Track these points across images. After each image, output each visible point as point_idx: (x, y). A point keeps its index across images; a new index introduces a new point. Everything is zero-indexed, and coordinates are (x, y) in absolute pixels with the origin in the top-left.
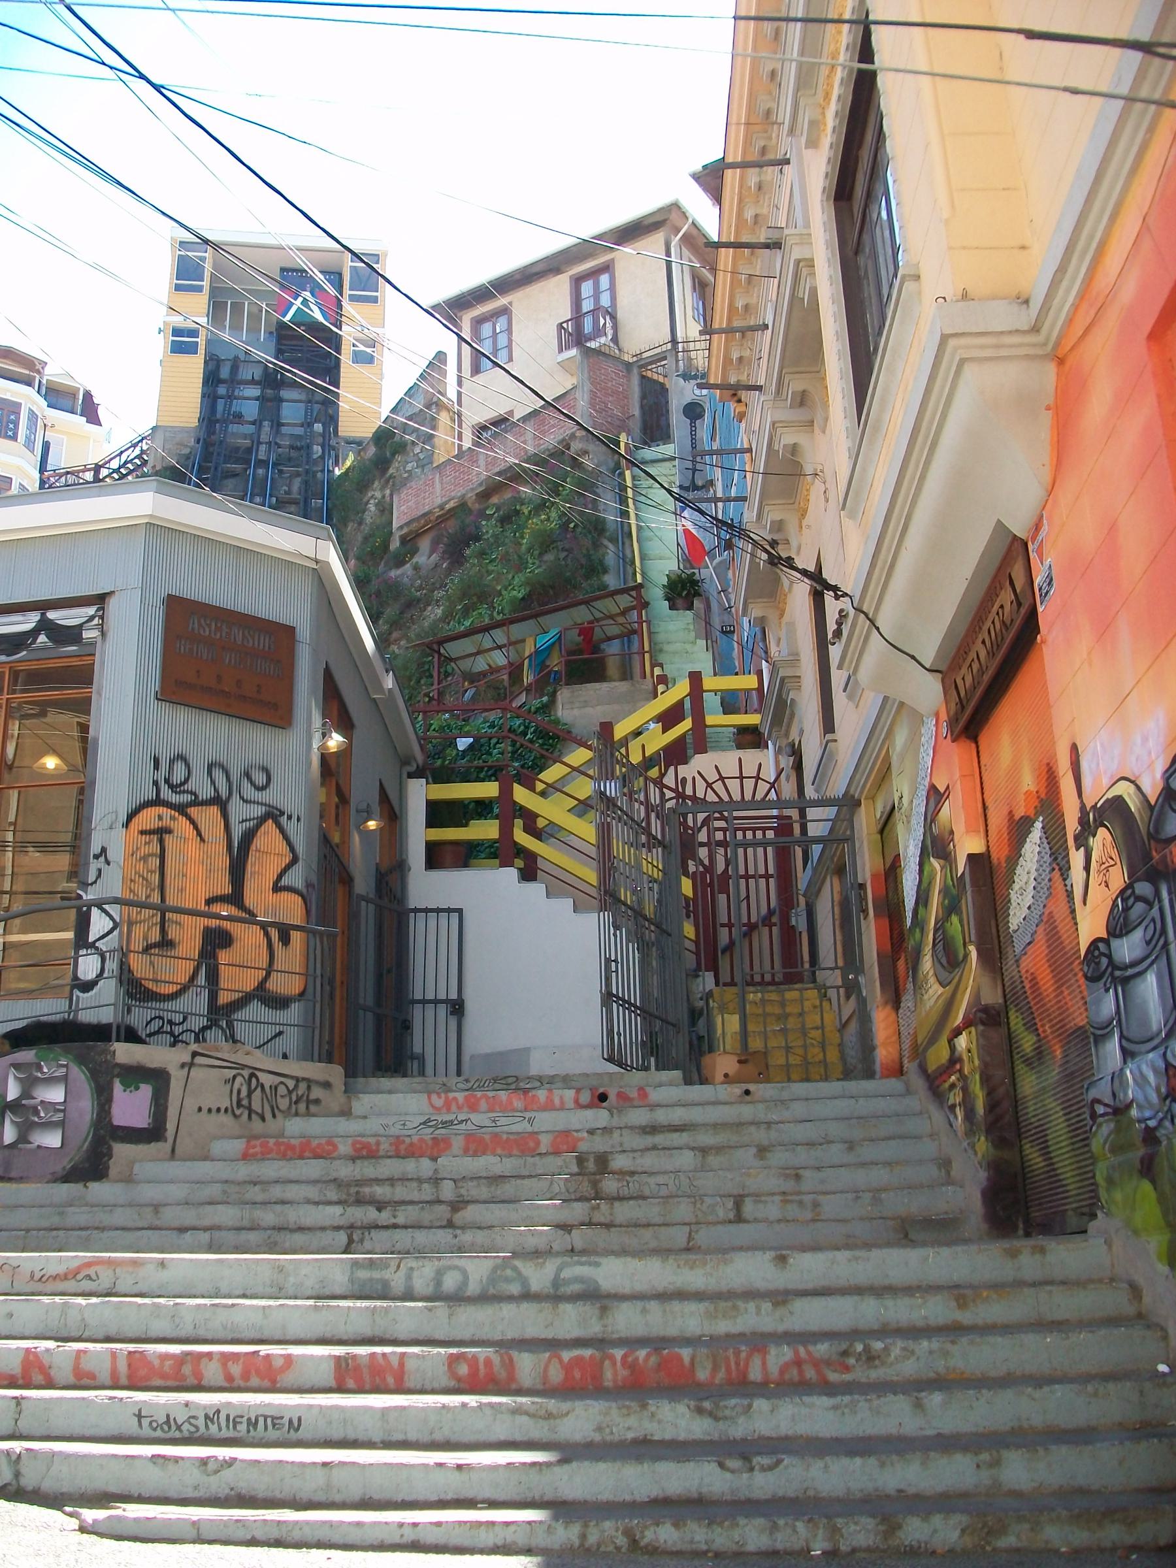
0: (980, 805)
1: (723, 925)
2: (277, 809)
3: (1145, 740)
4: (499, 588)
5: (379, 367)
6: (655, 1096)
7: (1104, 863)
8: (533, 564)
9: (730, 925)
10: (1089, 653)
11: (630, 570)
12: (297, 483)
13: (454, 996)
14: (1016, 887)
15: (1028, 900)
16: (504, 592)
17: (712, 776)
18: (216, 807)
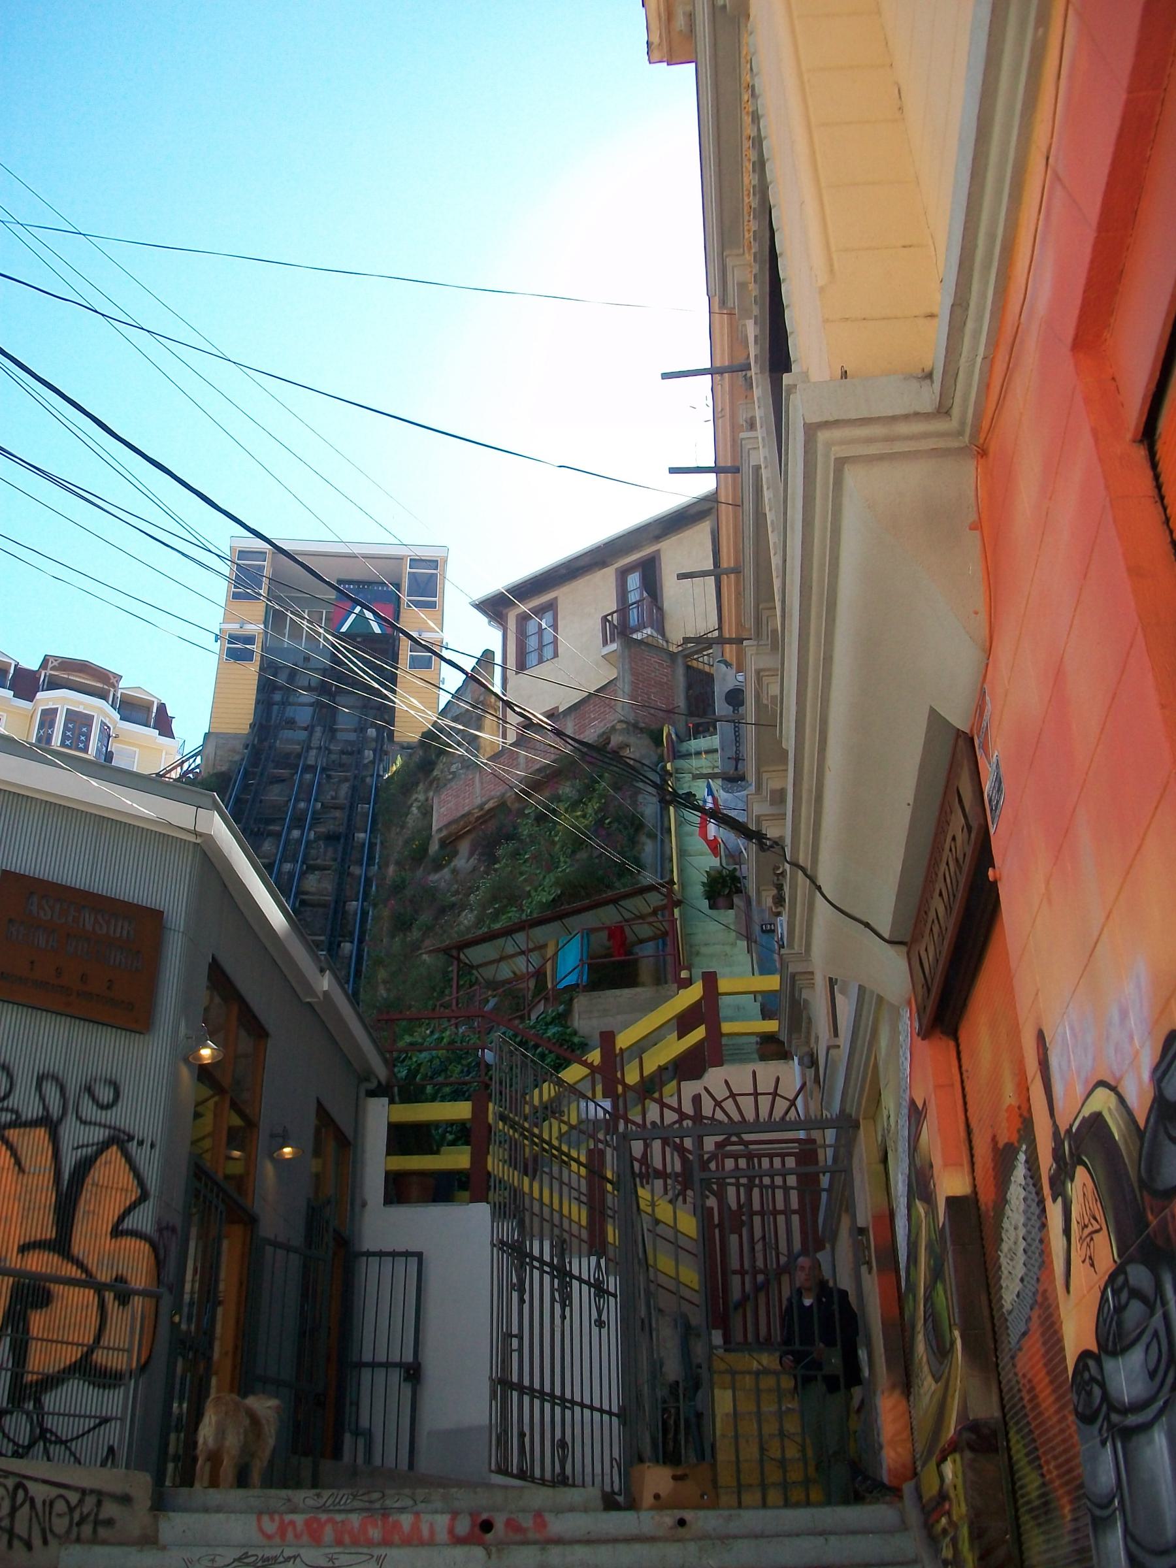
0: (962, 1127)
1: (735, 1272)
2: (124, 1132)
3: (1124, 1014)
4: (528, 888)
5: (437, 672)
6: (558, 1525)
7: (1086, 1226)
8: (565, 862)
9: (742, 1272)
10: (1048, 883)
11: (667, 865)
12: (345, 788)
13: (409, 1358)
14: (1005, 1247)
15: (1020, 1271)
16: (533, 893)
17: (721, 1093)
18: (43, 1130)
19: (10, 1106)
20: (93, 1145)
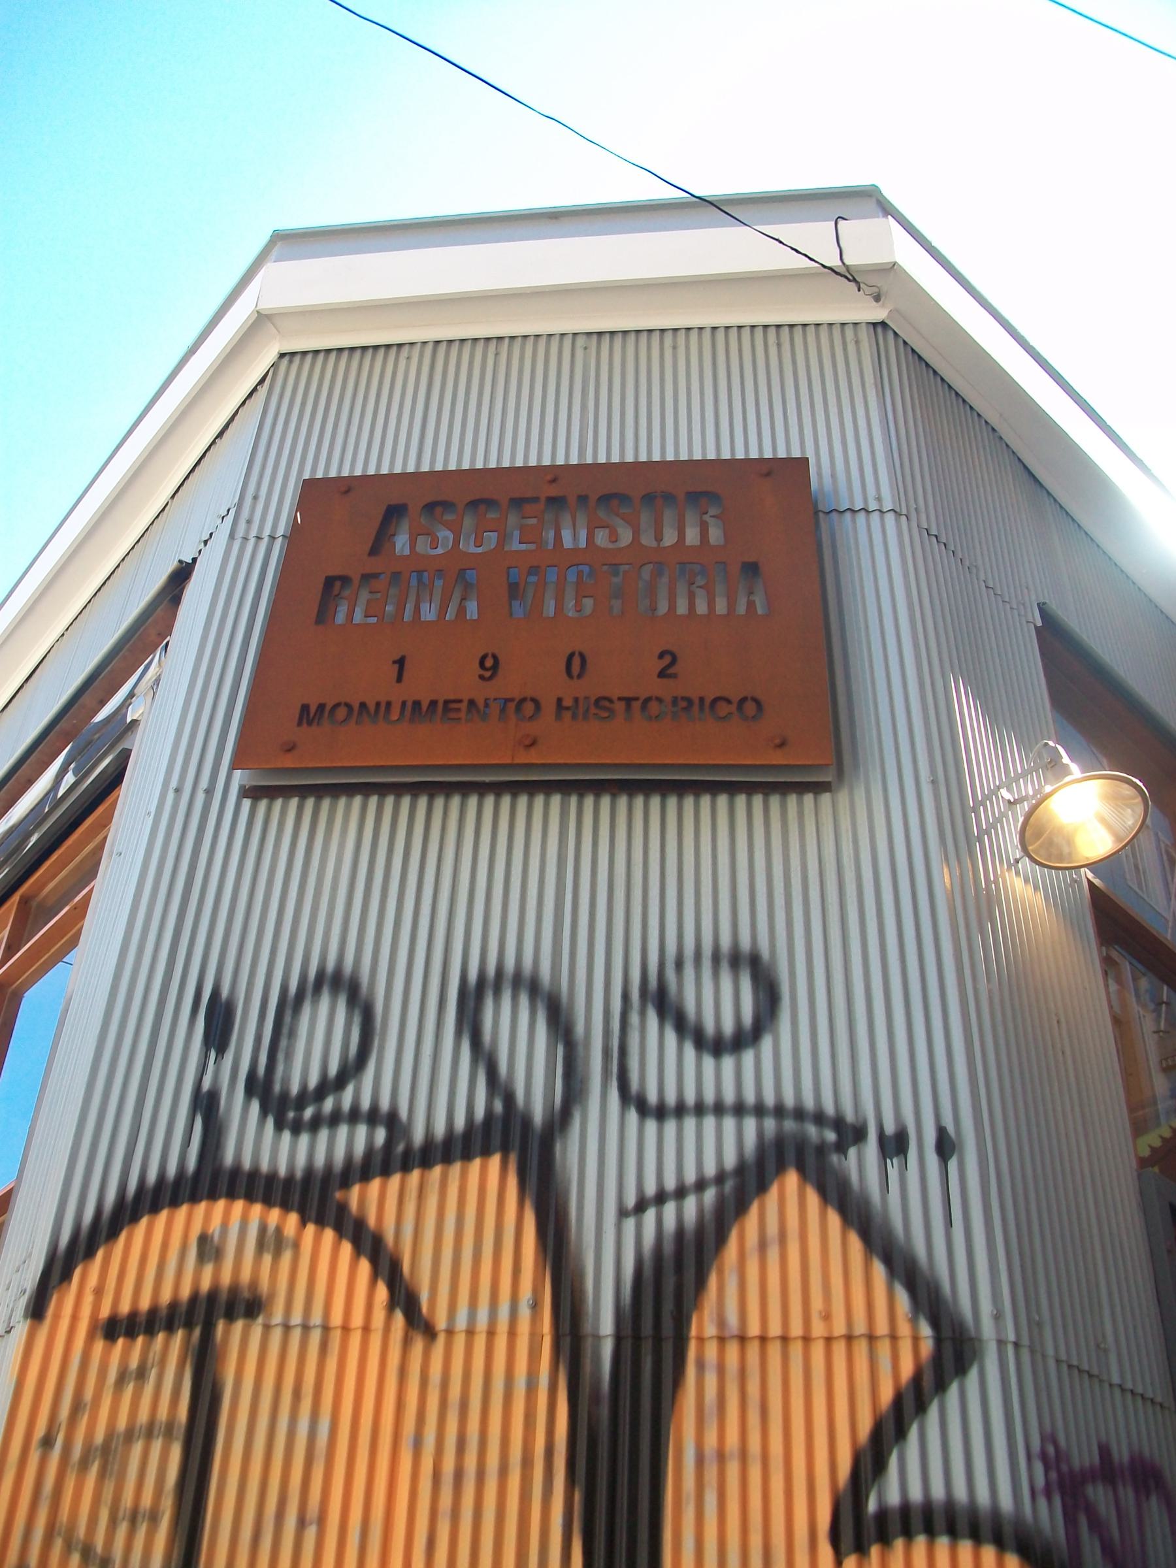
2: (819, 1118)
19: (366, 1104)
20: (701, 1185)
